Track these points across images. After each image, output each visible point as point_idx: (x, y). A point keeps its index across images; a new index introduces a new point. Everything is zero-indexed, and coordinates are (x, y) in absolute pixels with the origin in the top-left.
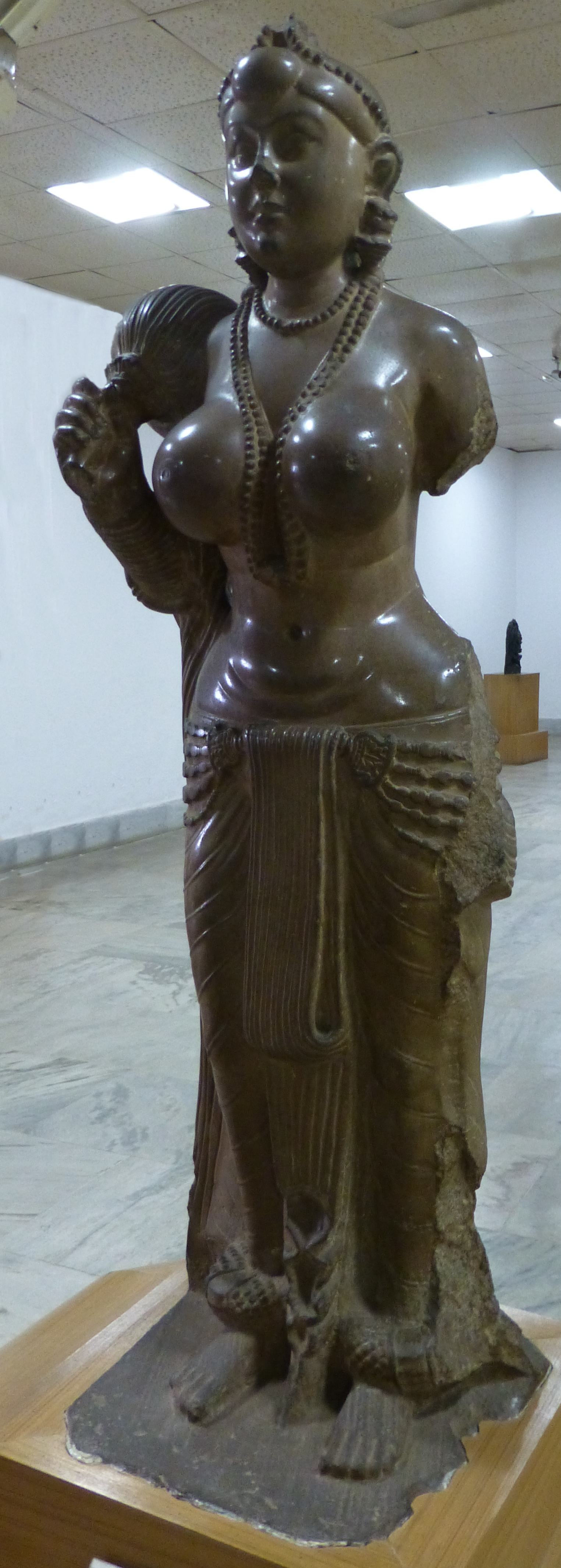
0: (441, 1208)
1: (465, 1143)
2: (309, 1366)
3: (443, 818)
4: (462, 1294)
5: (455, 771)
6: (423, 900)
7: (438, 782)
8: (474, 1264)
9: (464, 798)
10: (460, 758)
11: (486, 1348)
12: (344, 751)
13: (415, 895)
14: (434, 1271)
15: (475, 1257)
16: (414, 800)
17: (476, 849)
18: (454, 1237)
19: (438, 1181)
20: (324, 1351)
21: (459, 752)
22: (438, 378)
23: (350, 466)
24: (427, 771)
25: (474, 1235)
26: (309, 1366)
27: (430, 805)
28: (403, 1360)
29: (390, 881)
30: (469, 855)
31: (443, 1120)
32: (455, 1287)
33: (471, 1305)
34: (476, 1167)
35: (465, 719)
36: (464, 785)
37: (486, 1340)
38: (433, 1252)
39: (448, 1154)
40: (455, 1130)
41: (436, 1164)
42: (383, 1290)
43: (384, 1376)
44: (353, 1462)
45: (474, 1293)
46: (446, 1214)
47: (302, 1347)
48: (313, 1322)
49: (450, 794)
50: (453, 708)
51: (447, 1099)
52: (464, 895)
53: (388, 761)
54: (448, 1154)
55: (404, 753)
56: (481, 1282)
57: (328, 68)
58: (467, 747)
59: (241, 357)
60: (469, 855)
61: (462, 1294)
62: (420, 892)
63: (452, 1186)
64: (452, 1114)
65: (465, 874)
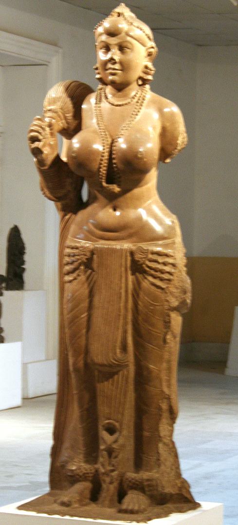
0: (161, 428)
1: (170, 402)
2: (109, 489)
3: (166, 276)
4: (168, 464)
5: (170, 260)
6: (157, 305)
7: (165, 264)
8: (173, 454)
9: (173, 271)
10: (172, 256)
12: (132, 253)
13: (155, 304)
15: (173, 451)
16: (156, 270)
17: (177, 288)
18: (165, 440)
19: (161, 415)
20: (116, 484)
21: (172, 254)
22: (168, 124)
23: (139, 156)
24: (160, 260)
25: (173, 443)
26: (109, 489)
27: (162, 272)
28: (148, 480)
29: (73, 376)
31: (163, 392)
32: (166, 460)
35: (174, 243)
36: (174, 265)
37: (176, 485)
38: (157, 445)
39: (164, 406)
40: (167, 396)
41: (160, 409)
42: (139, 464)
43: (139, 486)
44: (130, 508)
45: (173, 465)
46: (163, 429)
47: (108, 479)
49: (167, 268)
50: (170, 238)
51: (164, 384)
53: (147, 255)
54: (164, 406)
55: (153, 253)
58: (174, 253)
59: (100, 116)
60: (174, 290)
61: (168, 464)
62: (157, 303)
63: (165, 421)
64: (166, 390)
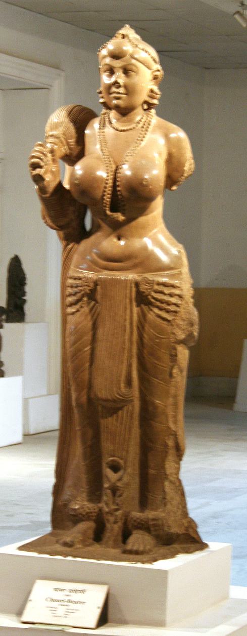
3: (172, 308)
4: (175, 502)
5: (177, 292)
7: (171, 295)
8: (179, 492)
9: (179, 302)
10: (179, 287)
11: (183, 528)
12: (137, 284)
14: (164, 491)
16: (161, 301)
17: (184, 320)
18: (171, 478)
19: (167, 452)
20: (120, 524)
21: (178, 285)
22: (174, 150)
23: (145, 183)
24: (167, 291)
25: (180, 481)
26: (114, 528)
27: (168, 303)
29: (76, 411)
30: (181, 323)
31: (169, 428)
32: (172, 499)
33: (178, 508)
34: (181, 451)
35: (180, 273)
36: (180, 296)
37: (183, 524)
39: (171, 443)
40: (173, 433)
41: (166, 446)
43: (144, 526)
44: (135, 548)
46: (169, 466)
47: (112, 519)
48: (117, 510)
49: (173, 300)
51: (171, 420)
52: (181, 336)
54: (171, 443)
55: (159, 284)
56: (182, 500)
57: (140, 48)
59: (104, 142)
60: (181, 323)
61: (175, 502)
63: (171, 458)
64: (172, 426)
65: (180, 329)
